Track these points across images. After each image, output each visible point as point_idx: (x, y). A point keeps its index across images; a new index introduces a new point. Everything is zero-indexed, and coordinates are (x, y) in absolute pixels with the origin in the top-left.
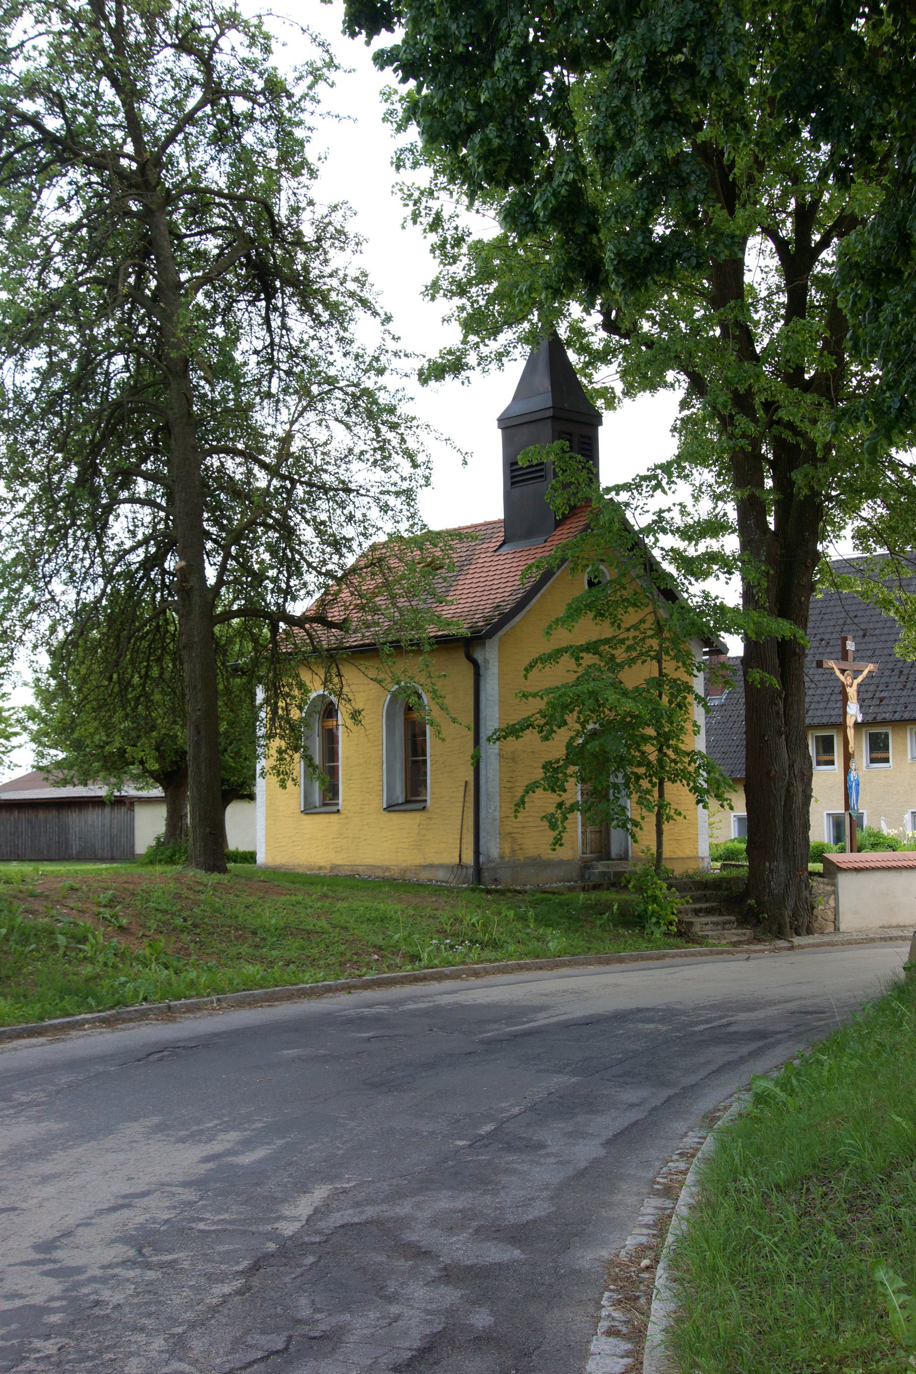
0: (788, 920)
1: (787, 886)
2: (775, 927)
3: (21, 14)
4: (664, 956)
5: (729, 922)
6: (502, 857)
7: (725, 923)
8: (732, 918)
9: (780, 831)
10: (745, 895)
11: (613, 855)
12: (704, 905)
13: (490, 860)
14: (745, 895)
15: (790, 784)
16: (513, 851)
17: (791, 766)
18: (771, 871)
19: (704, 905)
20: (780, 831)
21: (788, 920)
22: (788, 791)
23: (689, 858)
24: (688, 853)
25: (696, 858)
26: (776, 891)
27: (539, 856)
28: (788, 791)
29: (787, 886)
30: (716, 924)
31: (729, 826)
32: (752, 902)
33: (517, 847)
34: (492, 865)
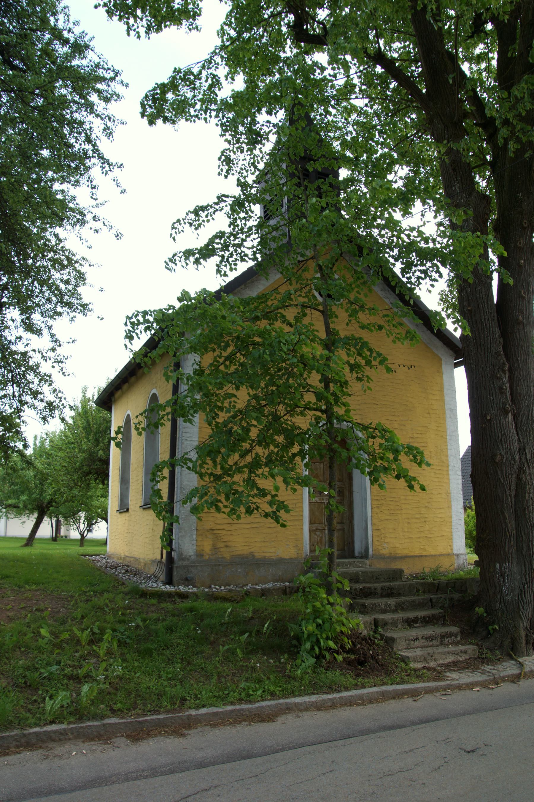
0: (523, 633)
1: (522, 592)
2: (507, 642)
3: (448, 286)
4: (190, 724)
5: (450, 635)
6: (199, 555)
7: (443, 637)
8: (455, 629)
9: (511, 525)
10: (475, 601)
11: (357, 554)
12: (421, 614)
13: (182, 558)
14: (475, 601)
15: (521, 470)
16: (215, 548)
17: (522, 450)
18: (503, 574)
19: (421, 614)
20: (511, 525)
21: (523, 633)
22: (519, 479)
23: (441, 555)
24: (441, 550)
25: (450, 555)
26: (509, 598)
27: (252, 554)
28: (519, 479)
29: (522, 592)
30: (430, 638)
31: (112, 505)
32: (480, 610)
33: (221, 545)
34: (185, 563)
